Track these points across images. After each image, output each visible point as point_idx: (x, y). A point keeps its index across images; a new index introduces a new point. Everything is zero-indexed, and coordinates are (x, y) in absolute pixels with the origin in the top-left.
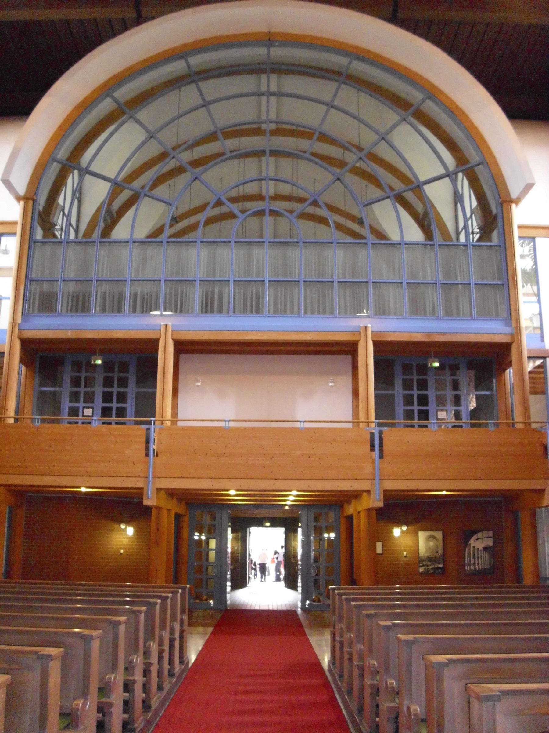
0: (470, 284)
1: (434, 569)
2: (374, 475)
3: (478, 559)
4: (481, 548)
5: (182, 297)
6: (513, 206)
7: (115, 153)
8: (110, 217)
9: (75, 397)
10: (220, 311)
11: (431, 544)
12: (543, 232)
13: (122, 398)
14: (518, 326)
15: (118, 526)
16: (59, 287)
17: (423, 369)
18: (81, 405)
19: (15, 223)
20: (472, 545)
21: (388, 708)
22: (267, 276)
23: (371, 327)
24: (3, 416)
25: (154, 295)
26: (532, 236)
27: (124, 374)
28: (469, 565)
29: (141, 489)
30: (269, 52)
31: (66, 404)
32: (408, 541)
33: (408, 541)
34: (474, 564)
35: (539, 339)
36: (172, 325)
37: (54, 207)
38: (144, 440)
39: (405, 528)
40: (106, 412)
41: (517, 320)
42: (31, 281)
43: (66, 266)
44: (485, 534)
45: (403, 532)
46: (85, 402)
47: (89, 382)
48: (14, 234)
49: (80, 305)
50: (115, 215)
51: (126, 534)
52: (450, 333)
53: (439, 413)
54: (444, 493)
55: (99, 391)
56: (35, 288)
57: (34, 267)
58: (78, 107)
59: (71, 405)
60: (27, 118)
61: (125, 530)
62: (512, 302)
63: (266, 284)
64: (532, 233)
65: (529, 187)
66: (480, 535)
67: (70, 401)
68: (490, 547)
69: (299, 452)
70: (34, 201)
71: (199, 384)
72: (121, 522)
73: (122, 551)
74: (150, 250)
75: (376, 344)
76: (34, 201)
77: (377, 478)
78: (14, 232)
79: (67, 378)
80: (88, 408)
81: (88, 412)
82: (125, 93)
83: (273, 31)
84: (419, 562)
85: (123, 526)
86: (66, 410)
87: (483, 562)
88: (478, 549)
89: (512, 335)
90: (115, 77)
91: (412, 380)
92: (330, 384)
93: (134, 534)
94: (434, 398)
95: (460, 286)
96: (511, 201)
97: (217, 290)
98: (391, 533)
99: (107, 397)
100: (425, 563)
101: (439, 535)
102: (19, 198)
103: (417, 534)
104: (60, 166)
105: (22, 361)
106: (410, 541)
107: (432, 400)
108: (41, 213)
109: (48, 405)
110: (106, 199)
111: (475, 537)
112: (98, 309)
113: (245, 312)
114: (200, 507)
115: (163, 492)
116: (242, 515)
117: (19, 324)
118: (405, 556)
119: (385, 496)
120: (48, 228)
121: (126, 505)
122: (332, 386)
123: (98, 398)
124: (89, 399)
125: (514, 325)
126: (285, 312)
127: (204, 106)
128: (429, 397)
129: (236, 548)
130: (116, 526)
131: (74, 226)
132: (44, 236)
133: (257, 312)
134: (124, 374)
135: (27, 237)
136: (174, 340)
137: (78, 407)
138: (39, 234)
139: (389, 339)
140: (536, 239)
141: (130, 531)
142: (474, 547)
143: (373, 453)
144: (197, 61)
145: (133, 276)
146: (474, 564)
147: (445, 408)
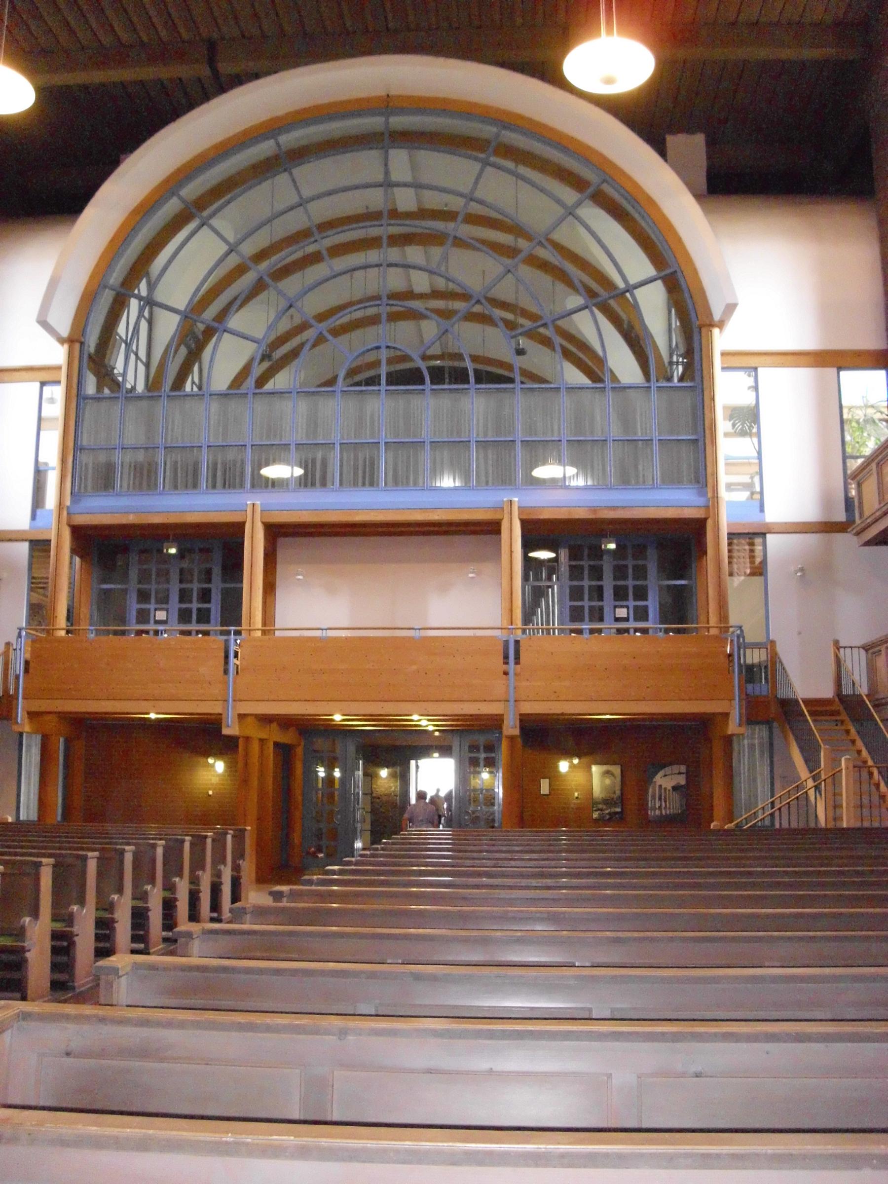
0: (652, 440)
2: (507, 692)
3: (665, 802)
4: (669, 788)
6: (716, 331)
7: (188, 268)
8: (195, 340)
9: (143, 596)
10: (324, 484)
11: (608, 781)
12: (768, 359)
13: (205, 596)
14: (716, 497)
15: (205, 760)
16: (117, 457)
17: (598, 553)
18: (152, 606)
19: (59, 368)
20: (658, 784)
21: (122, 853)
22: (384, 436)
23: (519, 501)
24: (51, 627)
25: (238, 465)
26: (753, 365)
27: (204, 568)
28: (654, 809)
29: (221, 714)
31: (133, 606)
32: (578, 778)
33: (578, 778)
34: (660, 807)
35: (758, 509)
36: (261, 504)
37: (111, 343)
38: (223, 654)
39: (576, 761)
40: (184, 616)
41: (713, 487)
43: (128, 428)
44: (675, 768)
45: (572, 766)
47: (164, 575)
48: (58, 382)
49: (145, 477)
50: (201, 337)
51: (215, 771)
52: (624, 507)
53: (617, 610)
55: (174, 589)
56: (86, 458)
59: (139, 606)
60: (74, 221)
61: (213, 766)
62: (708, 464)
63: (382, 447)
64: (752, 362)
65: (731, 308)
66: (668, 770)
67: (139, 602)
68: (682, 786)
69: (414, 667)
70: (82, 344)
71: (301, 577)
72: (207, 755)
73: (210, 793)
74: (233, 405)
75: (524, 523)
76: (82, 344)
77: (512, 700)
78: (57, 379)
79: (133, 574)
80: (622, 607)
81: (161, 615)
82: (192, 190)
84: (593, 804)
85: (211, 761)
87: (673, 806)
88: (665, 789)
89: (707, 507)
90: (179, 171)
92: (471, 575)
93: (225, 771)
94: (612, 591)
95: (640, 443)
96: (712, 325)
97: (319, 456)
98: (557, 767)
99: (184, 596)
100: (600, 806)
101: (616, 770)
102: (62, 341)
103: (591, 768)
104: (114, 293)
105: (74, 551)
106: (583, 778)
107: (608, 593)
108: (92, 356)
109: (110, 611)
110: (175, 334)
112: (167, 486)
113: (355, 484)
114: (307, 736)
116: (398, 743)
117: (68, 507)
118: (577, 798)
119: (521, 721)
120: (105, 375)
121: (202, 735)
122: (472, 578)
123: (174, 597)
124: (163, 600)
125: (710, 495)
126: (408, 484)
127: (301, 205)
128: (605, 588)
129: (393, 789)
130: (202, 760)
131: (144, 360)
132: (99, 389)
133: (372, 484)
134: (204, 568)
135: (74, 392)
136: (263, 523)
137: (149, 610)
138: (91, 386)
139: (542, 517)
140: (759, 369)
141: (219, 766)
142: (660, 786)
144: (290, 139)
145: (211, 440)
147: (625, 603)
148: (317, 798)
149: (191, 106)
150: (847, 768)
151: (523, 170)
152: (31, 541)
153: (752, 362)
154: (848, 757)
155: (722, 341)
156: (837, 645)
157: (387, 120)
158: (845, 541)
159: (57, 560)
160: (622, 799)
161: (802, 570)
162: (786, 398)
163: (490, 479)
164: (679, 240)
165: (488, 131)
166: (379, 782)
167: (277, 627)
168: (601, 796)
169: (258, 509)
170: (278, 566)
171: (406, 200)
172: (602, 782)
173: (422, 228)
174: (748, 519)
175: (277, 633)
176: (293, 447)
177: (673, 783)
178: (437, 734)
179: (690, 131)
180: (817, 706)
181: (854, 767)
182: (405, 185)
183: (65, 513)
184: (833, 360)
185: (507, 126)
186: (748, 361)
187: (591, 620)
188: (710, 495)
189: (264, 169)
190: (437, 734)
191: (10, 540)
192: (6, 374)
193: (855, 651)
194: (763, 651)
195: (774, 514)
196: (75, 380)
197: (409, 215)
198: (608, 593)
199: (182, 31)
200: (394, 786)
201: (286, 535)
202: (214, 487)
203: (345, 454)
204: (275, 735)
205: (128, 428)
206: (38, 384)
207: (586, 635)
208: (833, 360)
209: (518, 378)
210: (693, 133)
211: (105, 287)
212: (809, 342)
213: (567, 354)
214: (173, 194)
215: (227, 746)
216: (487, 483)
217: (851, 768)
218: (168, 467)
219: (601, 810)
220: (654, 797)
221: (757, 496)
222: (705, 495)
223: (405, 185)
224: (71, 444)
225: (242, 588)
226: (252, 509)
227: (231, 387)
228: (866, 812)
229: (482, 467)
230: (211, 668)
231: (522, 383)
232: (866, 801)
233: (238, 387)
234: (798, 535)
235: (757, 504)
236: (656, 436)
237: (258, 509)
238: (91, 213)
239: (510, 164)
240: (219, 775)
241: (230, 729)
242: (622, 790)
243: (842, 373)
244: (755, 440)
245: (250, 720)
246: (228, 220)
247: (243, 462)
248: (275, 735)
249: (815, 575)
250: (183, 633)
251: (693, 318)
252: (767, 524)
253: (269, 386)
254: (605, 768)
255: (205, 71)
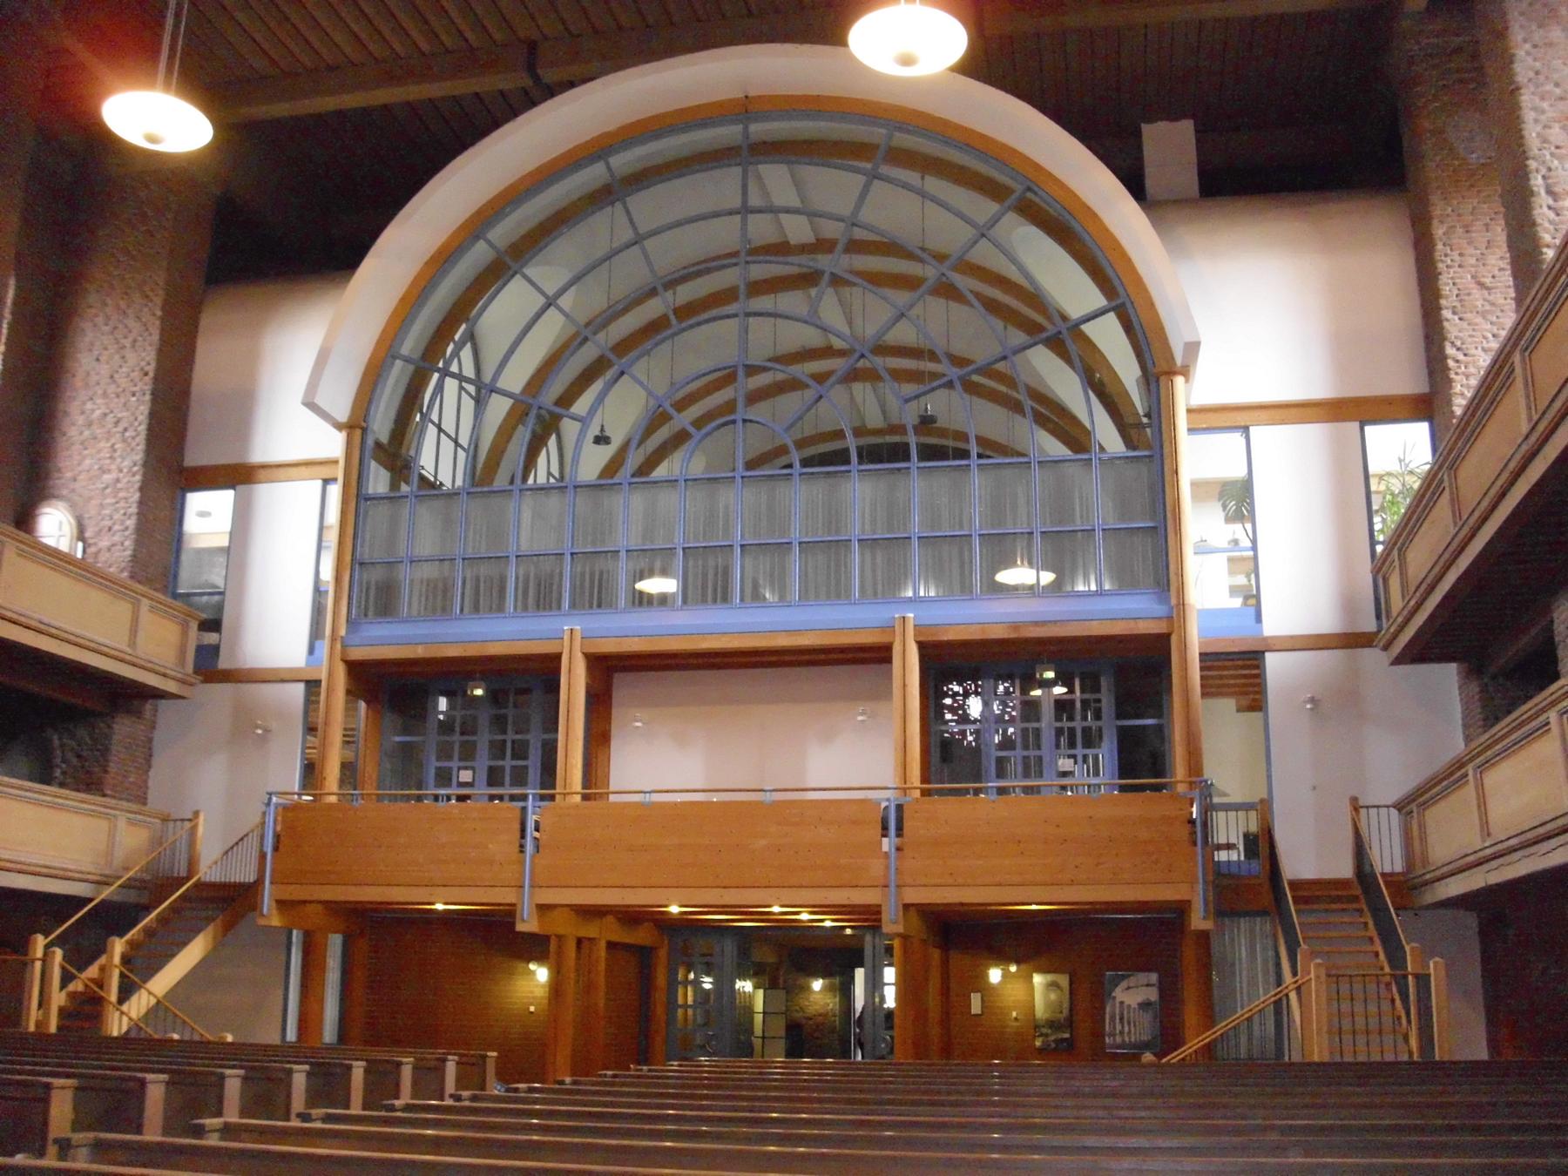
1: (1057, 1041)
2: (886, 876)
4: (1134, 1005)
5: (600, 580)
6: (1179, 381)
7: (520, 327)
8: (538, 419)
9: (445, 753)
11: (1053, 996)
12: (1263, 415)
13: (520, 752)
14: (1182, 605)
18: (454, 764)
19: (336, 462)
30: (608, 165)
31: (433, 765)
34: (1122, 1033)
39: (1013, 968)
40: (494, 778)
42: (361, 564)
44: (1142, 977)
45: (1006, 975)
46: (461, 759)
54: (1034, 907)
55: (483, 739)
57: (368, 537)
58: (433, 261)
59: (439, 764)
61: (533, 973)
69: (763, 842)
70: (364, 430)
73: (532, 1009)
75: (922, 646)
77: (893, 884)
80: (466, 768)
81: (466, 776)
82: (504, 232)
83: (752, 94)
85: (532, 966)
86: (432, 772)
89: (1170, 618)
91: (451, 744)
96: (1171, 373)
98: (985, 976)
100: (1044, 1030)
101: (1064, 980)
102: (339, 426)
106: (1022, 991)
107: (1048, 737)
109: (406, 770)
111: (1124, 984)
113: (704, 601)
115: (913, 911)
121: (494, 935)
124: (468, 754)
132: (394, 486)
135: (353, 491)
137: (450, 769)
143: (885, 840)
146: (1122, 1033)
148: (686, 1019)
149: (496, 124)
150: (1318, 977)
151: (933, 184)
152: (308, 682)
153: (1241, 419)
154: (1319, 961)
155: (1188, 394)
156: (1356, 806)
157: (746, 128)
158: (1374, 660)
159: (328, 706)
160: (1070, 1023)
161: (1312, 700)
162: (1288, 465)
163: (880, 587)
164: (1128, 260)
165: (877, 134)
166: (812, 998)
167: (612, 788)
168: (1047, 1016)
169: (578, 636)
170: (614, 711)
171: (798, 230)
172: (1046, 997)
173: (796, 268)
174: (1234, 635)
175: (612, 798)
176: (623, 554)
177: (1140, 999)
178: (848, 931)
179: (1174, 117)
180: (1314, 893)
181: (1329, 976)
182: (788, 211)
183: (339, 646)
184: (1354, 411)
185: (902, 127)
186: (1215, 418)
187: (512, 785)
188: (1173, 601)
189: (602, 197)
190: (848, 931)
191: (283, 681)
192: (282, 470)
193: (1383, 811)
194: (1253, 814)
195: (1273, 626)
196: (355, 476)
197: (804, 249)
198: (1048, 737)
199: (444, 37)
200: (831, 1003)
201: (625, 669)
202: (525, 608)
203: (691, 563)
204: (610, 931)
205: (424, 534)
206: (319, 483)
207: (264, 808)
208: (1354, 411)
209: (974, 450)
210: (1176, 119)
211: (394, 358)
212: (1319, 390)
213: (1041, 420)
214: (477, 238)
215: (536, 947)
216: (875, 594)
217: (1323, 978)
218: (468, 586)
219: (1046, 1035)
220: (1113, 1018)
221: (1253, 601)
222: (1166, 600)
223: (788, 211)
224: (348, 558)
225: (556, 740)
226: (571, 635)
227: (601, 476)
228: (1347, 1038)
229: (868, 573)
230: (501, 845)
231: (980, 456)
232: (1347, 1025)
233: (647, 474)
234: (1325, 652)
235: (1252, 611)
236: (795, 535)
237: (578, 636)
238: (370, 266)
239: (912, 177)
240: (543, 986)
241: (528, 923)
242: (1071, 1010)
243: (1368, 429)
244: (1249, 526)
245: (913, 911)
246: (548, 271)
247: (561, 574)
248: (610, 931)
249: (1333, 707)
250: (492, 798)
251: (1160, 364)
252: (1266, 639)
253: (661, 472)
254: (1050, 977)
255: (528, 82)
